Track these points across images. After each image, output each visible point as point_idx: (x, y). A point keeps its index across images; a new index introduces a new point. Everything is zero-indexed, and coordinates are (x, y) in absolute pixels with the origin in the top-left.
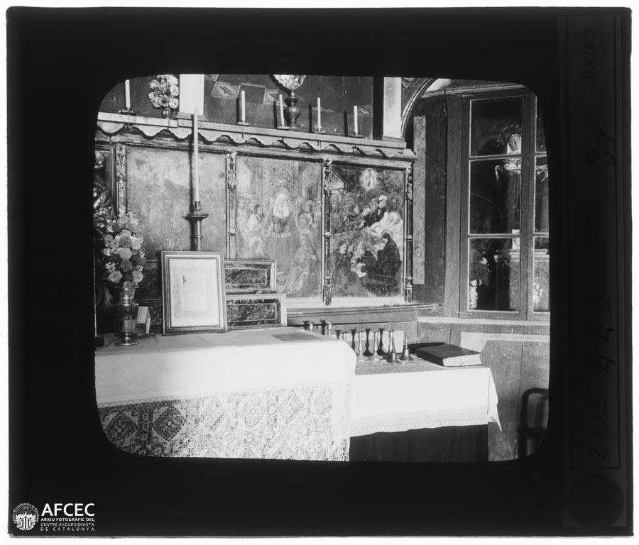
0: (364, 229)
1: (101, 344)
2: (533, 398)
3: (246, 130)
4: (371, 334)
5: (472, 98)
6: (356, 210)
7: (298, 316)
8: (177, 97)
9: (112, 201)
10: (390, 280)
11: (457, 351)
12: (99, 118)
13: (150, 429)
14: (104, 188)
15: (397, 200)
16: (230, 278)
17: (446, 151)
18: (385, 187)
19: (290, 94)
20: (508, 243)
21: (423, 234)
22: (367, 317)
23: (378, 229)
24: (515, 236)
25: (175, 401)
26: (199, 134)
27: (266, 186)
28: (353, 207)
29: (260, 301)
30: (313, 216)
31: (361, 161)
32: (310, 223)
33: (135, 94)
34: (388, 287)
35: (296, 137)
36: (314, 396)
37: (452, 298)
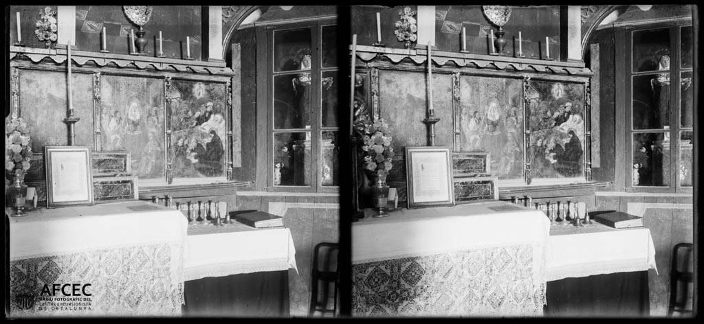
0: (555, 128)
1: (362, 216)
2: (681, 250)
3: (467, 56)
4: (561, 205)
5: (274, 29)
6: (549, 114)
7: (147, 193)
8: (416, 33)
9: (369, 111)
10: (574, 165)
11: (624, 217)
12: (11, 50)
13: (36, 277)
14: (363, 101)
15: (579, 106)
16: (96, 165)
17: (256, 68)
18: (570, 96)
19: (139, 29)
20: (661, 135)
21: (240, 130)
22: (558, 193)
23: (565, 127)
24: (308, 131)
25: (54, 257)
26: (432, 60)
27: (482, 98)
28: (188, 111)
29: (479, 182)
30: (517, 119)
31: (193, 77)
32: (156, 123)
33: (24, 32)
34: (573, 170)
35: (503, 61)
36: (520, 251)
37: (620, 178)
